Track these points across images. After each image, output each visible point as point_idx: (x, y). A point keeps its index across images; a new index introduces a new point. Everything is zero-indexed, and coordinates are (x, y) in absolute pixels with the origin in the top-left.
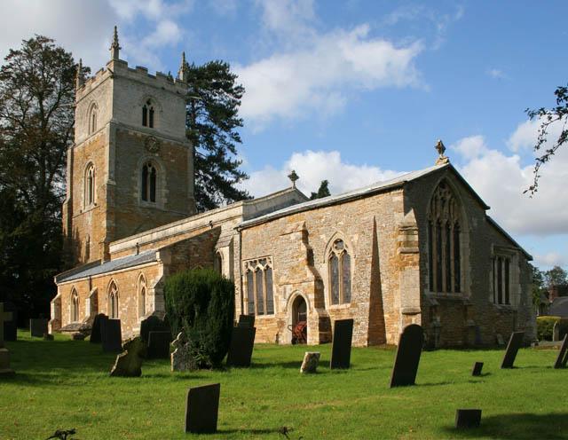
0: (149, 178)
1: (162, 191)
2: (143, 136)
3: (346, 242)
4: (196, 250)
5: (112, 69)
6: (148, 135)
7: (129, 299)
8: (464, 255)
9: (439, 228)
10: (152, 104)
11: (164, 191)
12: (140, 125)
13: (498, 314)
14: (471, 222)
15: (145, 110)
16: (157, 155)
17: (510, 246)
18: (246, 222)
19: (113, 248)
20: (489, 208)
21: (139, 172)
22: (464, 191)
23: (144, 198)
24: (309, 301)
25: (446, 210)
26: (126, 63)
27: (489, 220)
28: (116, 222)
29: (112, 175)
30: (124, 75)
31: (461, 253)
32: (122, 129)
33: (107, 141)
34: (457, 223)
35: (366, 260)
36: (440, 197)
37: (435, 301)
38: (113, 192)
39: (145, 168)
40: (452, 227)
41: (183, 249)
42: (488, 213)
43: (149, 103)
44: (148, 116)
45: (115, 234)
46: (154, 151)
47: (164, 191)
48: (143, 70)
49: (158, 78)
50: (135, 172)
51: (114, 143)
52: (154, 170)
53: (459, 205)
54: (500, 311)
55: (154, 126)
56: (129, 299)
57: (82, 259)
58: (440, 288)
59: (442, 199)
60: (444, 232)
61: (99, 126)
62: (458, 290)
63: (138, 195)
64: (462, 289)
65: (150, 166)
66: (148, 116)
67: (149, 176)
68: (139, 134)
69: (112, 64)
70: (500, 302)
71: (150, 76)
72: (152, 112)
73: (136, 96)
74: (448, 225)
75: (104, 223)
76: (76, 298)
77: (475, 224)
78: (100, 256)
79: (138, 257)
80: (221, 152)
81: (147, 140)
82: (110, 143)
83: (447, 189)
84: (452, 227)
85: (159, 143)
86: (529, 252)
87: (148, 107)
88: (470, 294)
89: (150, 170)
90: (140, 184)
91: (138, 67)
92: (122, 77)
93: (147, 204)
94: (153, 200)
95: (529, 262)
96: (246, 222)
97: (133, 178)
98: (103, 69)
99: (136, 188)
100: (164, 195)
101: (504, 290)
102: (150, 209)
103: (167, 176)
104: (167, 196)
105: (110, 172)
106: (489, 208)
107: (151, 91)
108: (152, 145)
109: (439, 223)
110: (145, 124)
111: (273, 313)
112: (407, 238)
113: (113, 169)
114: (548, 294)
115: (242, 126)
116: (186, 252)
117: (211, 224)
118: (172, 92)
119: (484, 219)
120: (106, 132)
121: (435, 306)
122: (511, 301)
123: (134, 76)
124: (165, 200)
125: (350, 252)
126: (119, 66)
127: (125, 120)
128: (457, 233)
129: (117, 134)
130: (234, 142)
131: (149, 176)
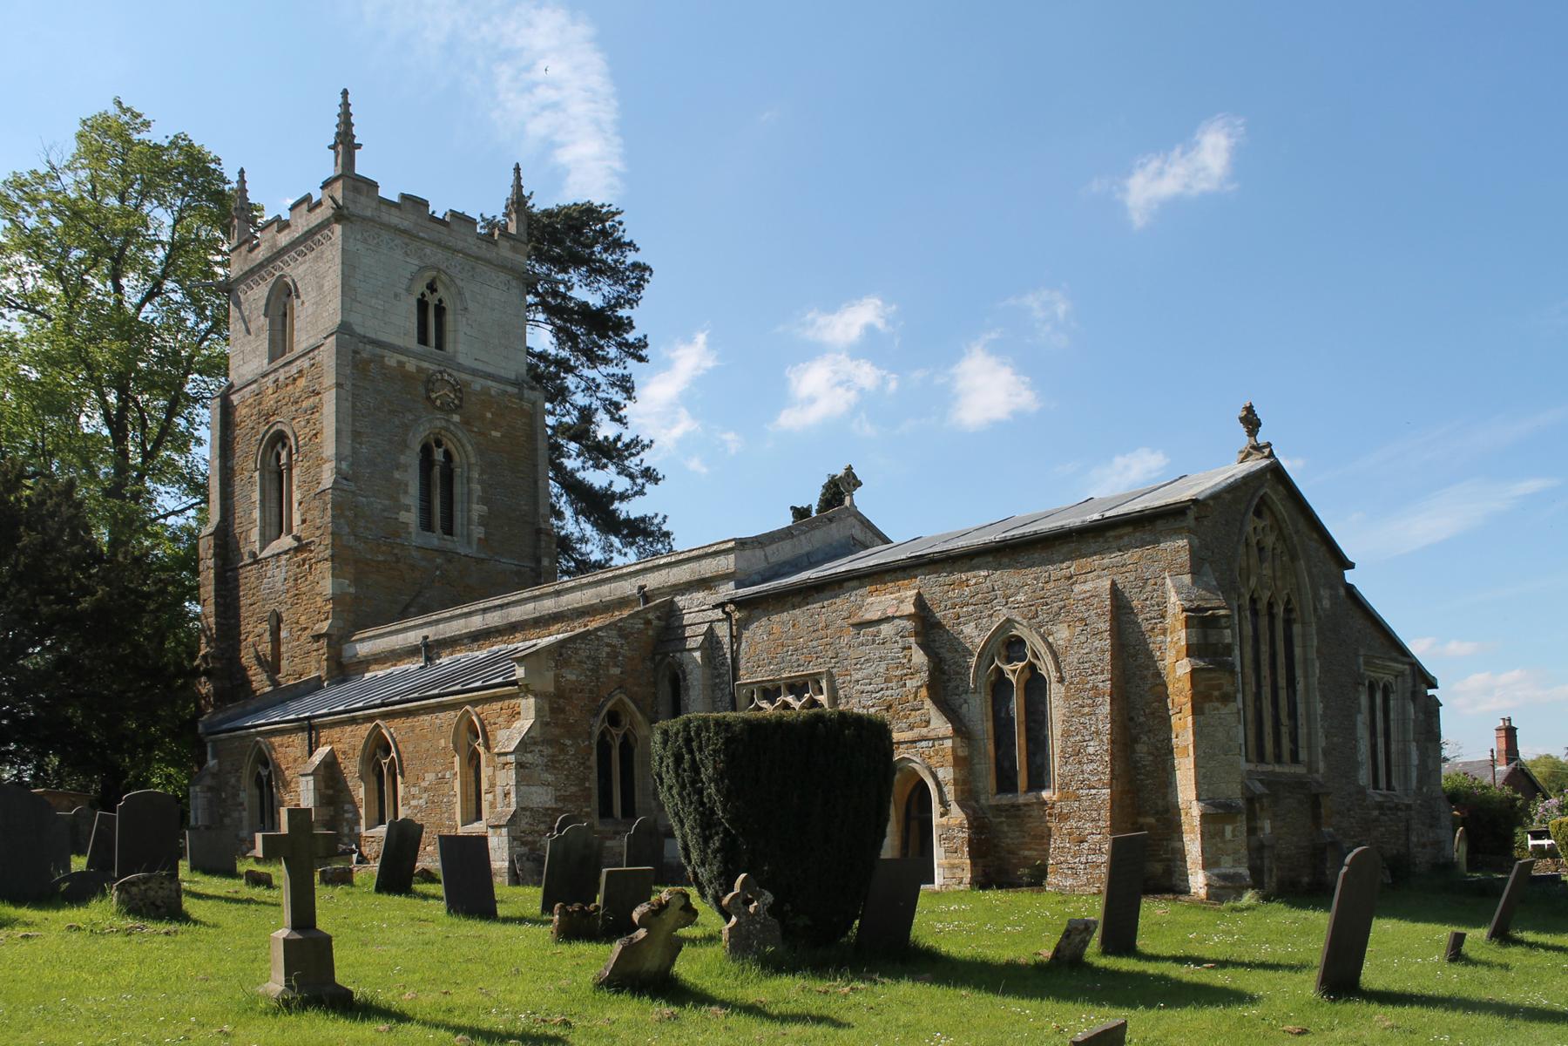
0: (438, 474)
1: (472, 510)
2: (420, 370)
3: (1033, 641)
4: (613, 655)
5: (339, 196)
6: (434, 367)
7: (430, 777)
8: (1306, 677)
9: (1255, 613)
10: (442, 292)
11: (478, 509)
12: (412, 342)
13: (1376, 813)
14: (1317, 598)
15: (422, 305)
16: (456, 418)
17: (1395, 654)
18: (742, 592)
19: (365, 646)
20: (1351, 566)
21: (412, 459)
22: (1302, 524)
23: (427, 525)
24: (938, 784)
25: (1267, 571)
26: (374, 185)
27: (1350, 590)
28: (357, 581)
29: (344, 465)
30: (369, 213)
31: (1299, 672)
32: (367, 351)
33: (330, 379)
34: (1289, 601)
35: (1095, 688)
36: (1254, 541)
37: (1258, 784)
38: (346, 502)
39: (426, 451)
40: (1280, 610)
41: (583, 654)
42: (1350, 576)
43: (432, 287)
44: (431, 318)
45: (358, 612)
46: (447, 409)
47: (478, 509)
48: (415, 204)
49: (455, 227)
50: (402, 459)
51: (348, 386)
52: (448, 455)
53: (1294, 558)
54: (1380, 806)
55: (449, 347)
56: (430, 777)
57: (260, 681)
58: (1261, 758)
59: (1258, 543)
60: (1264, 622)
61: (302, 341)
62: (1295, 758)
63: (411, 517)
64: (1303, 755)
65: (439, 444)
66: (431, 318)
67: (437, 470)
68: (411, 365)
69: (339, 185)
70: (1376, 786)
71: (433, 218)
72: (440, 310)
73: (400, 268)
74: (1271, 605)
75: (327, 586)
76: (264, 773)
77: (1326, 603)
78: (316, 669)
79: (432, 674)
80: (586, 415)
81: (429, 382)
82: (339, 385)
83: (1267, 522)
84: (1280, 610)
85: (459, 388)
86: (1431, 668)
87: (432, 300)
88: (1321, 766)
89: (438, 455)
90: (414, 488)
91: (404, 197)
92: (364, 219)
93: (435, 539)
94: (448, 530)
95: (1430, 692)
96: (742, 592)
97: (397, 475)
98: (308, 198)
99: (406, 500)
100: (475, 517)
101: (1381, 757)
102: (441, 552)
103: (482, 472)
104: (484, 521)
105: (339, 457)
106: (1351, 566)
107: (436, 256)
108: (441, 393)
109: (1253, 601)
110: (423, 340)
111: (479, 818)
112: (1205, 636)
113: (347, 451)
114: (847, 757)
115: (641, 359)
116: (589, 665)
117: (645, 595)
118: (488, 262)
119: (1342, 592)
120: (327, 356)
121: (1261, 797)
122: (1394, 783)
123: (394, 218)
124: (478, 532)
125: (1047, 667)
126: (356, 190)
127: (368, 326)
128: (1288, 623)
129: (355, 366)
130: (617, 396)
131: (437, 470)
